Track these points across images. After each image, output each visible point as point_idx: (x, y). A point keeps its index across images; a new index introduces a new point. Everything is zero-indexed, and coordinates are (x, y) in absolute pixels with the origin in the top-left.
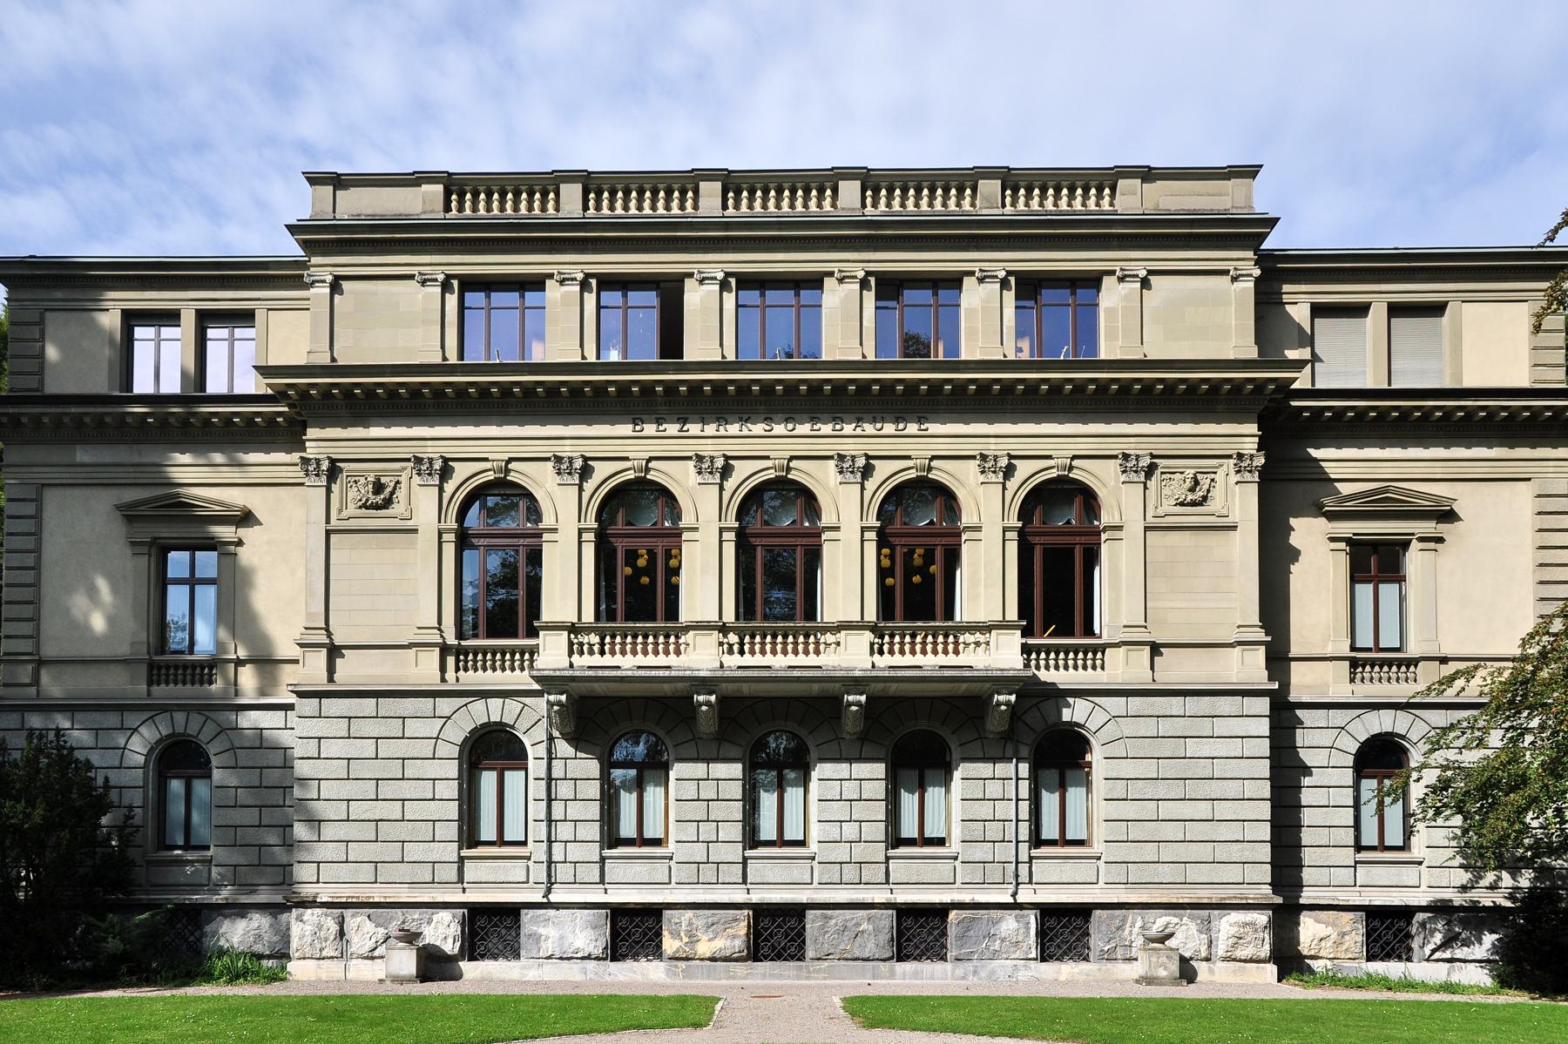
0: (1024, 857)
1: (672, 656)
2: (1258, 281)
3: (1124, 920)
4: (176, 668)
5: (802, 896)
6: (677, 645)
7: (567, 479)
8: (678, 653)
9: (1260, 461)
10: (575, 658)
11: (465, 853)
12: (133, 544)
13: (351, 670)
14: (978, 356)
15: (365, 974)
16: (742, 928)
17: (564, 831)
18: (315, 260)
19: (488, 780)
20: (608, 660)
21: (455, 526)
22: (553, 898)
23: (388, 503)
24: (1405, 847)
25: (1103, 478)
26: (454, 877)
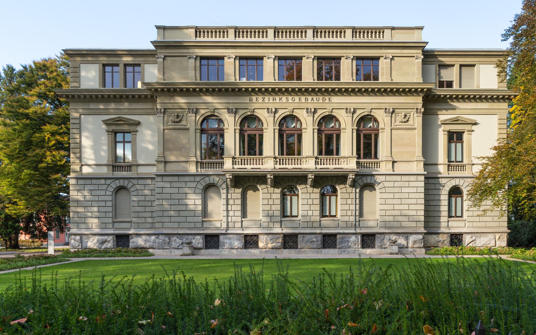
0: (357, 220)
1: (261, 165)
2: (423, 59)
3: (384, 237)
4: (120, 167)
5: (297, 231)
6: (262, 162)
7: (388, 114)
8: (262, 164)
9: (423, 110)
10: (317, 166)
11: (282, 219)
12: (108, 131)
13: (400, 168)
14: (385, 81)
15: (176, 254)
16: (280, 240)
17: (231, 213)
18: (159, 51)
19: (453, 199)
20: (243, 166)
21: (200, 128)
22: (229, 232)
23: (180, 121)
24: (462, 216)
25: (379, 115)
26: (200, 226)
